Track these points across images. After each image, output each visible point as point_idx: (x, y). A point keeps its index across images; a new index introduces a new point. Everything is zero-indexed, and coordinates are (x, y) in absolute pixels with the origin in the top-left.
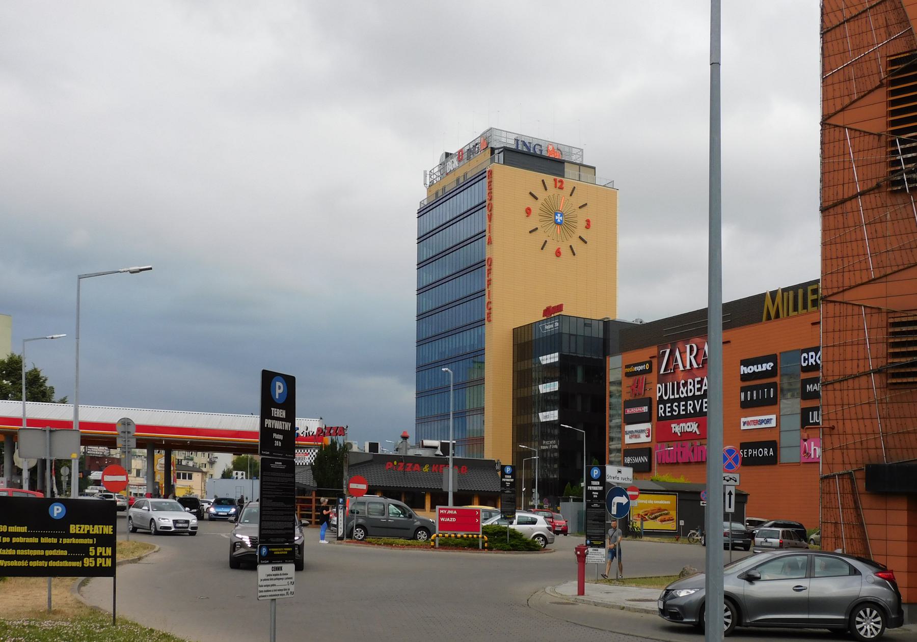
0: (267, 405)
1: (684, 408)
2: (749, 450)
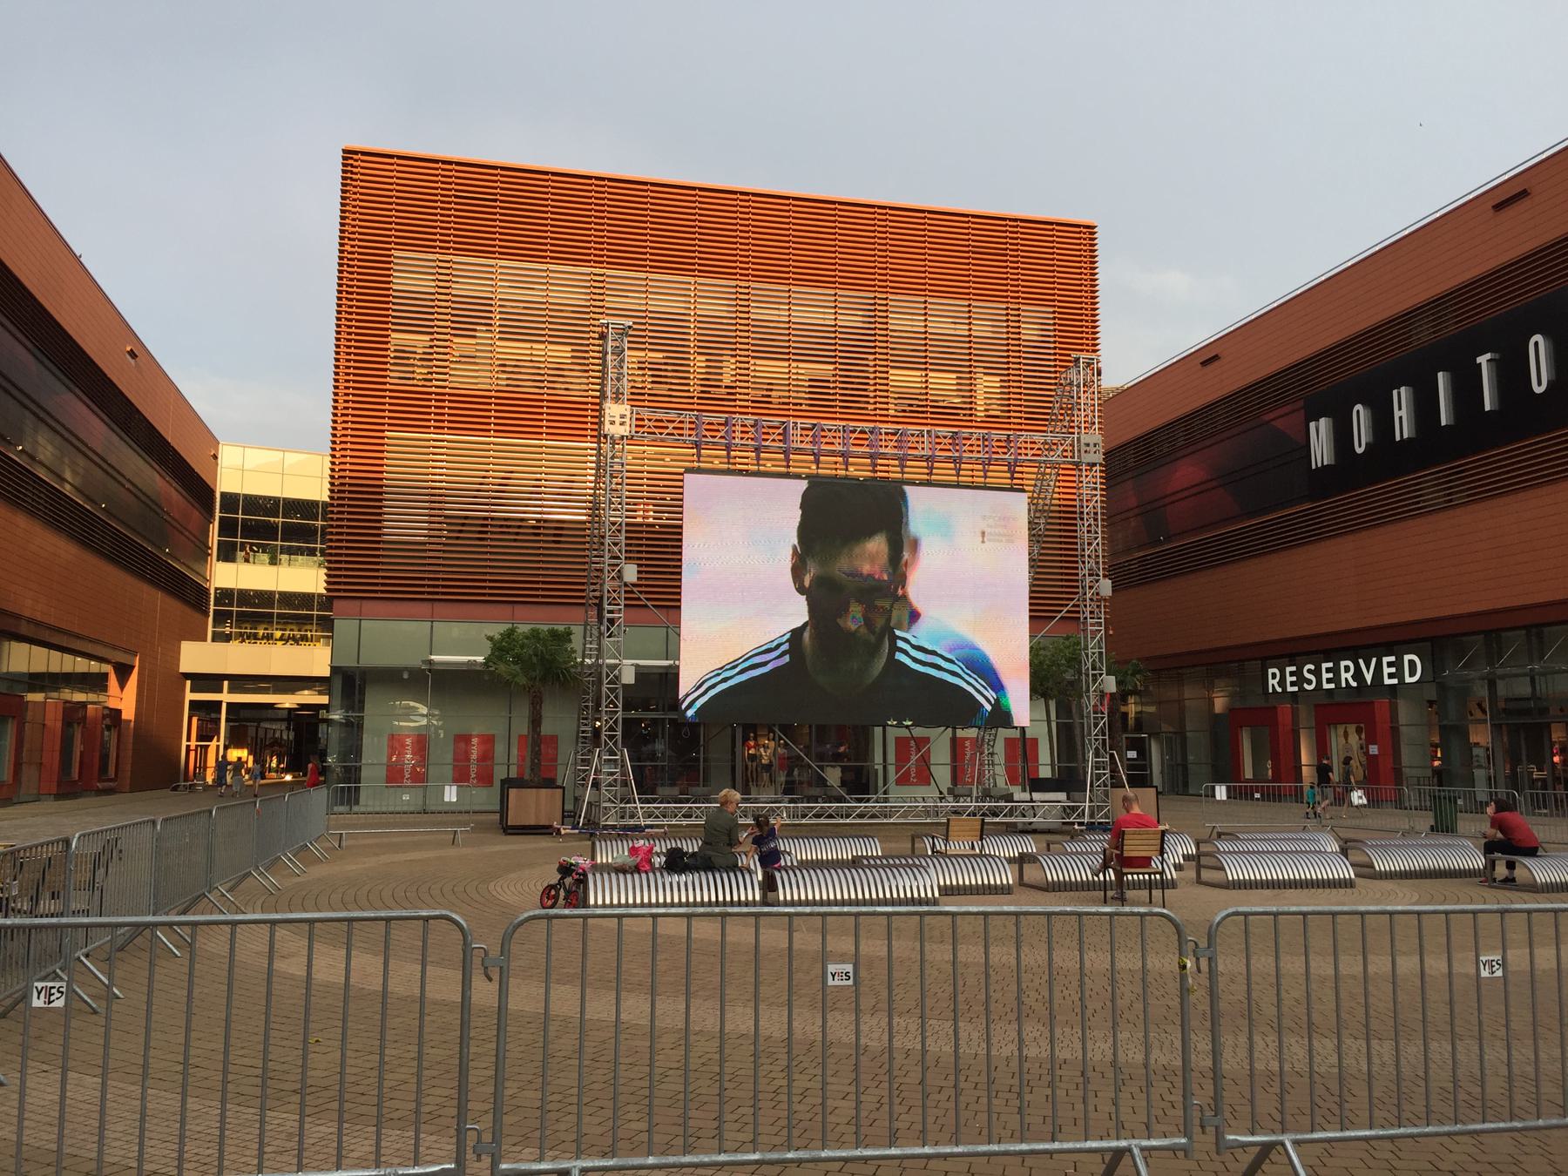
0: (392, 750)
2: (1343, 664)
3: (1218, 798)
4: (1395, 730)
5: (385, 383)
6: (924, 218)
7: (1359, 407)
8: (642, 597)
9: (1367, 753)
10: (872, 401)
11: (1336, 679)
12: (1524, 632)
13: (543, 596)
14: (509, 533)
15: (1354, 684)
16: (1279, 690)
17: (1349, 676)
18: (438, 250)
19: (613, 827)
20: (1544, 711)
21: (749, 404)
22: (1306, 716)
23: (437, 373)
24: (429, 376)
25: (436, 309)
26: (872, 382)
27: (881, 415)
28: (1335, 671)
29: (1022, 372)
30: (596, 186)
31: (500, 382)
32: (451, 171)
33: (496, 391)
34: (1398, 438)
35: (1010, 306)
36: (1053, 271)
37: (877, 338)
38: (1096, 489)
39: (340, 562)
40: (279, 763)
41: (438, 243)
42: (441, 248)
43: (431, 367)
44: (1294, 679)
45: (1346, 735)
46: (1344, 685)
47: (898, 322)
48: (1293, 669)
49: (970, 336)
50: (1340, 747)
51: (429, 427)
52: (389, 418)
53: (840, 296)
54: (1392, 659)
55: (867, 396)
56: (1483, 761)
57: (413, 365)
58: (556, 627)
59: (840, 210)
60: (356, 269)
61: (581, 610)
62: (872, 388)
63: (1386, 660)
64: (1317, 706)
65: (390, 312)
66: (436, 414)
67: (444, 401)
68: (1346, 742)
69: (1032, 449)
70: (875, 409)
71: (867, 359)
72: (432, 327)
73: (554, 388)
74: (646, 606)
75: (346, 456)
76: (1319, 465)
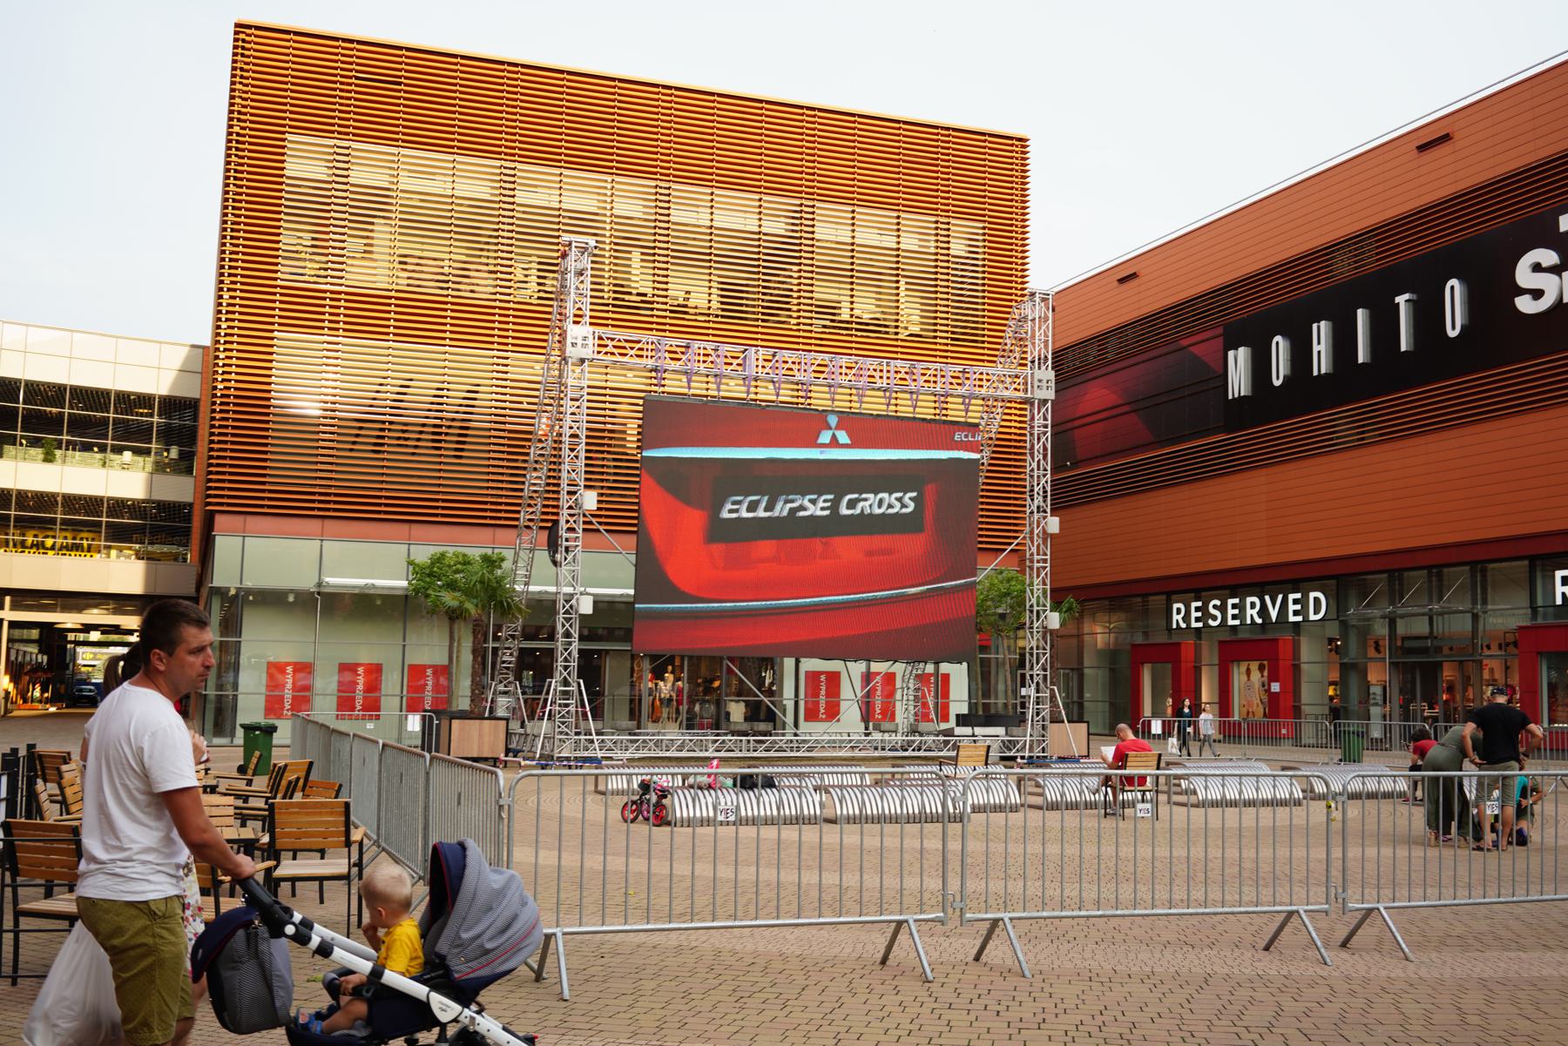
2: (1249, 600)
3: (1153, 732)
4: (1296, 668)
5: (276, 279)
6: (614, 87)
7: (1278, 338)
9: (1268, 691)
10: (795, 315)
11: (1240, 616)
12: (1467, 568)
13: (443, 515)
14: (407, 446)
15: (1259, 621)
17: (1254, 612)
18: (336, 135)
19: (568, 759)
20: (1438, 650)
21: (668, 314)
22: (1209, 656)
23: (333, 270)
24: (322, 273)
25: (333, 200)
26: (795, 295)
27: (804, 331)
28: (1241, 607)
29: (761, 269)
30: (509, 72)
31: (400, 281)
32: (288, 41)
33: (397, 291)
34: (1315, 373)
35: (804, 202)
36: (760, 154)
37: (803, 248)
39: (224, 473)
40: (44, 691)
41: (336, 128)
42: (339, 133)
44: (1199, 614)
45: (1248, 672)
46: (1249, 622)
47: (824, 232)
48: (1199, 604)
51: (323, 328)
52: (451, 332)
53: (403, 156)
54: (1298, 596)
55: (789, 310)
56: (1379, 699)
57: (305, 260)
59: (719, 102)
60: (246, 153)
61: (513, 532)
62: (795, 301)
63: (1292, 597)
64: (1221, 643)
65: (283, 201)
66: (331, 314)
67: (339, 300)
68: (1249, 683)
69: (641, 349)
70: (799, 324)
71: (791, 270)
72: (328, 219)
73: (459, 290)
74: (598, 531)
75: (231, 358)
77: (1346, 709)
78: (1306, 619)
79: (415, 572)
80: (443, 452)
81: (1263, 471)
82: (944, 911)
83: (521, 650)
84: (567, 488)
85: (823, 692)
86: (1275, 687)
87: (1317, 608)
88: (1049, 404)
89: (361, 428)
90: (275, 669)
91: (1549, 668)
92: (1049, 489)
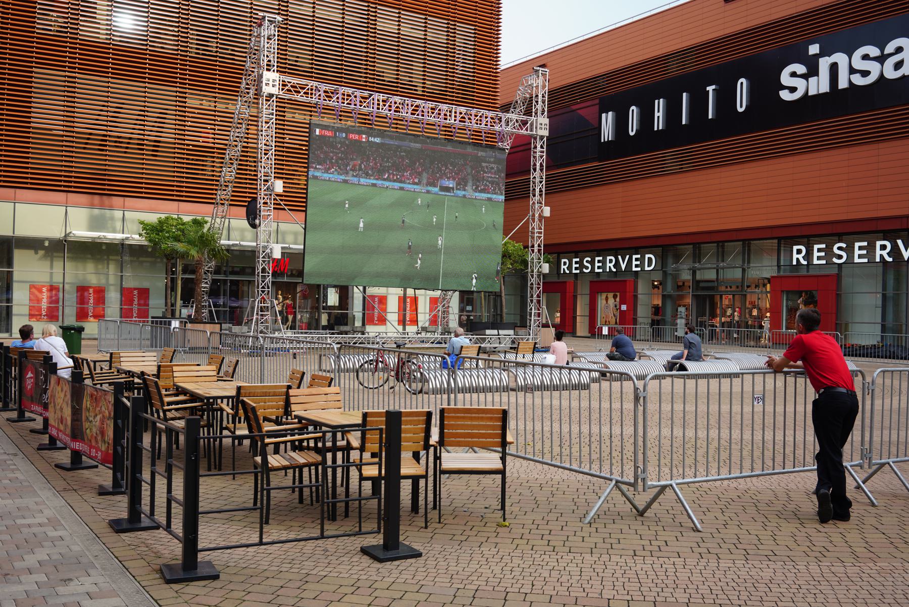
1: (600, 264)
2: (608, 258)
3: (604, 333)
4: (636, 297)
8: (282, 203)
11: (603, 267)
15: (614, 270)
16: (568, 272)
22: (583, 291)
28: (603, 262)
34: (656, 129)
38: (273, 115)
43: (67, 18)
44: (578, 266)
45: (607, 299)
46: (608, 270)
49: (343, 22)
50: (603, 306)
54: (639, 256)
56: (684, 315)
58: (198, 218)
61: (212, 206)
63: (634, 257)
64: (591, 282)
68: (607, 305)
74: (284, 209)
76: (606, 140)
77: (664, 320)
78: (643, 270)
79: (144, 229)
80: (144, 152)
81: (621, 185)
82: (862, 459)
83: (213, 280)
84: (263, 178)
85: (136, 302)
86: (624, 307)
87: (650, 263)
88: (545, 139)
89: (91, 134)
90: (35, 288)
91: (787, 300)
92: (544, 190)
